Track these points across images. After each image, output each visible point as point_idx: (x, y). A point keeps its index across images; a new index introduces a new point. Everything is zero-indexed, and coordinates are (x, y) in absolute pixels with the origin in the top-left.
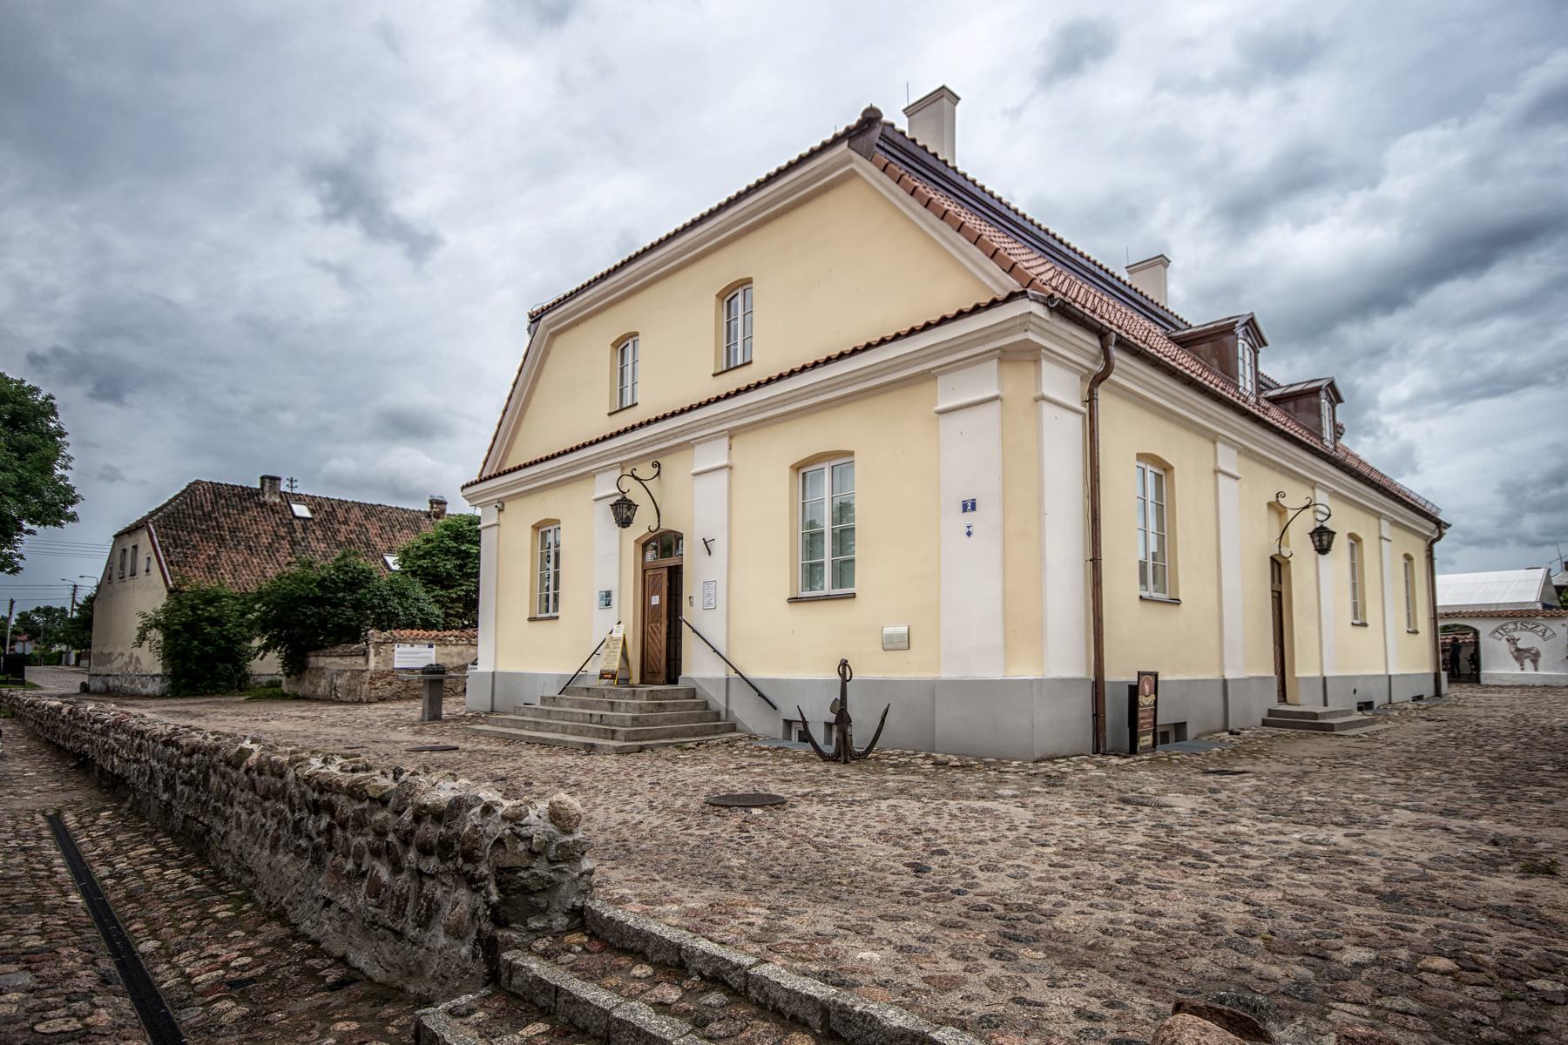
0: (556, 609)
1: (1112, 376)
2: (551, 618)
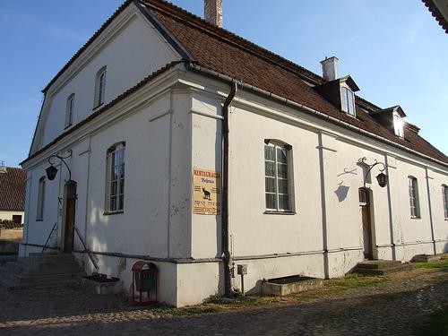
0: (121, 207)
1: (235, 98)
2: (118, 213)
